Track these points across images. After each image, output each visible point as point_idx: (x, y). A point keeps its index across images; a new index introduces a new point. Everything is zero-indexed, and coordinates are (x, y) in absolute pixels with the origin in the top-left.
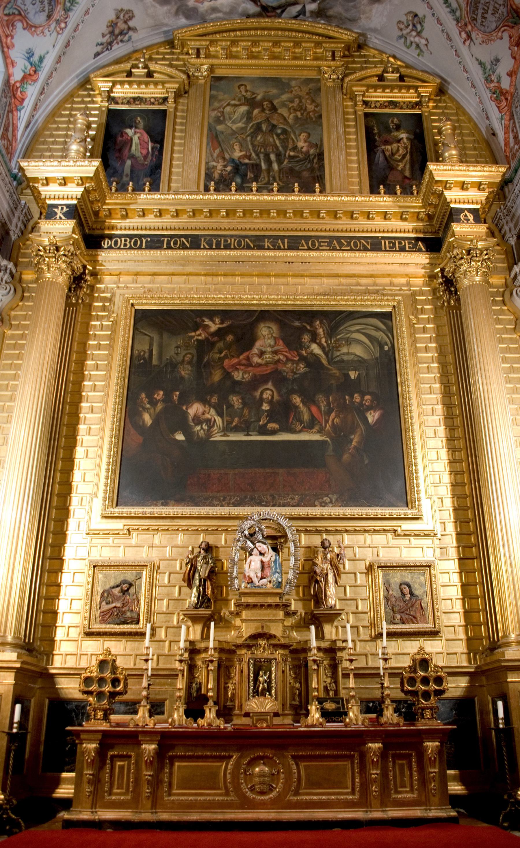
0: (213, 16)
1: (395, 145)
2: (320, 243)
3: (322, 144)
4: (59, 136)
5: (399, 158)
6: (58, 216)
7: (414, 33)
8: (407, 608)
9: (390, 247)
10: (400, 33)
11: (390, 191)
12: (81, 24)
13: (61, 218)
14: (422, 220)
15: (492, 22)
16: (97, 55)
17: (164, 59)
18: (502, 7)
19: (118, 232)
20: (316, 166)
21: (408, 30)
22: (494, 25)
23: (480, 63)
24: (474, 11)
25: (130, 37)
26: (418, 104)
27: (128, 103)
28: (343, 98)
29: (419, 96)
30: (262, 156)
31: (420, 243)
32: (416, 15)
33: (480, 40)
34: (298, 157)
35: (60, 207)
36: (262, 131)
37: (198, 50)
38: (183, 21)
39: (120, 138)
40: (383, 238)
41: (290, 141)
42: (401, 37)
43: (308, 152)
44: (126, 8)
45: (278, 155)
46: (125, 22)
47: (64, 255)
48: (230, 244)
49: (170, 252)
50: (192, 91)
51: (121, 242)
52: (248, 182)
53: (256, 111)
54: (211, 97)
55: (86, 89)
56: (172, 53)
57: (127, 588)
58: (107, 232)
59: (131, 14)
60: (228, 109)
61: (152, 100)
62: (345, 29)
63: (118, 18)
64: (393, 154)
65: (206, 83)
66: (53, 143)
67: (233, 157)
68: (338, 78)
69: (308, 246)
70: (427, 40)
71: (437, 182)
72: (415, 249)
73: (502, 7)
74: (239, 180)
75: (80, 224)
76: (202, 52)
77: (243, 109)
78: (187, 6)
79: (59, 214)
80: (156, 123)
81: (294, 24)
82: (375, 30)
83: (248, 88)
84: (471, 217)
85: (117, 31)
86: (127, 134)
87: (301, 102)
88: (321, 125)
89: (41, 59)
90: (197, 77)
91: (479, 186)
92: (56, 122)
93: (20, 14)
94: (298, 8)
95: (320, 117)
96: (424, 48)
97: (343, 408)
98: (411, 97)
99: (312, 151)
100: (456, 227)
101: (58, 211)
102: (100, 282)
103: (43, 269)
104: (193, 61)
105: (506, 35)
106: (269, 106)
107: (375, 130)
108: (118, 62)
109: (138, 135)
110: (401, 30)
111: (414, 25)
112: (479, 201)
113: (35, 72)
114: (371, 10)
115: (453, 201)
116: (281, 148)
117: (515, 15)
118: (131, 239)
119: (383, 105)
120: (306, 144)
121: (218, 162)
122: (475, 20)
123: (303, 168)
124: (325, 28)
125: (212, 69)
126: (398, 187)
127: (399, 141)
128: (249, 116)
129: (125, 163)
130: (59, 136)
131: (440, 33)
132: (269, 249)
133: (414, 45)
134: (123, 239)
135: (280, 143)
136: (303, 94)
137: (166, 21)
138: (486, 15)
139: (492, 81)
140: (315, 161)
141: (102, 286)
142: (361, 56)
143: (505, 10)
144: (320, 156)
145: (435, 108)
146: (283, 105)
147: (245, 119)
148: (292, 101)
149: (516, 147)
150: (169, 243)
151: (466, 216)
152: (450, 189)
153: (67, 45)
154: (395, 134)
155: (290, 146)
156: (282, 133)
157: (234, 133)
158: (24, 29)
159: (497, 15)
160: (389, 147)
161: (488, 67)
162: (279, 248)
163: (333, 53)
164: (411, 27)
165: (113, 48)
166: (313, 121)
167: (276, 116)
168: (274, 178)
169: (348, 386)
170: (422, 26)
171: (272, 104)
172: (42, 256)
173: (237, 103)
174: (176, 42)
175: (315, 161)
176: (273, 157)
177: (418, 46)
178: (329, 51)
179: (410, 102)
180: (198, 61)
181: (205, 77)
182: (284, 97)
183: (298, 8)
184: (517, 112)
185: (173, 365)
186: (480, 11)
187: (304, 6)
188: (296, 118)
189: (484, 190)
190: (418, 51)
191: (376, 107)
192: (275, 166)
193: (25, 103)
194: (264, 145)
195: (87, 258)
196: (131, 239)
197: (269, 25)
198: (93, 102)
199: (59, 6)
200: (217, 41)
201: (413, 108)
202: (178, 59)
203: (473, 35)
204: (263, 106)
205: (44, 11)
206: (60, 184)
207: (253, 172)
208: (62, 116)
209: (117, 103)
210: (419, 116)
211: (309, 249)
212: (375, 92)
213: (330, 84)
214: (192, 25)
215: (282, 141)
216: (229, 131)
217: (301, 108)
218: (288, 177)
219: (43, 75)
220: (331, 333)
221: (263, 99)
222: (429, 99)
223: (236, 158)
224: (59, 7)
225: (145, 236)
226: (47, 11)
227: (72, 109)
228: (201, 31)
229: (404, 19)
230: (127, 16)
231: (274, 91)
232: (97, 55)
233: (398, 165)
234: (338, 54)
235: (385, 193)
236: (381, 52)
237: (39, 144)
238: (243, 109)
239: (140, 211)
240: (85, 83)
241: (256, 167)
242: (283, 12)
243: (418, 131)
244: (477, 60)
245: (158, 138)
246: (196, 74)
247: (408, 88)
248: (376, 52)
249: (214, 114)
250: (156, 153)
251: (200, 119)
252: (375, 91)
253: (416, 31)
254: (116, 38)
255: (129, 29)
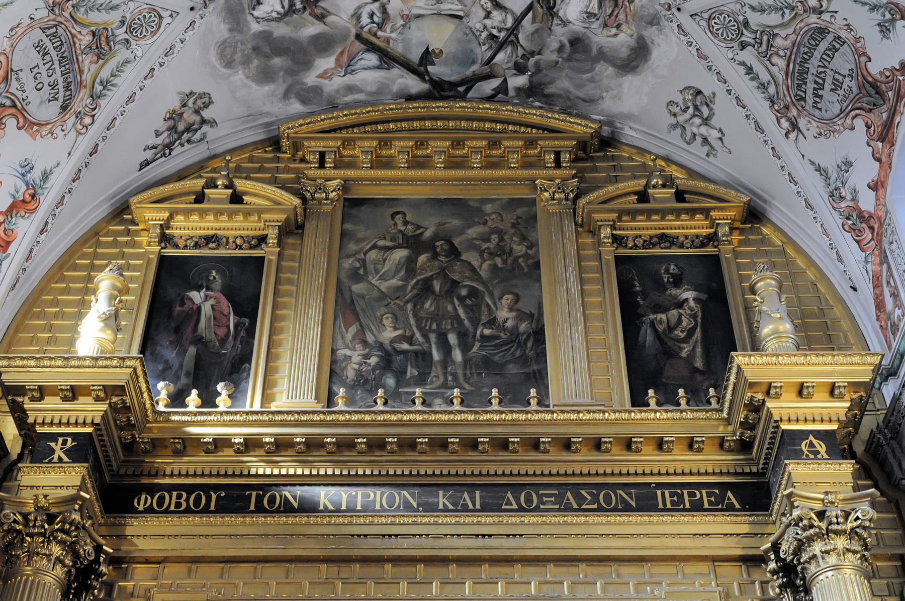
0: (349, 98)
1: (674, 313)
2: (540, 497)
3: (541, 314)
4: (69, 304)
5: (683, 335)
6: (56, 457)
7: (697, 121)
9: (672, 502)
10: (673, 121)
11: (668, 399)
12: (119, 118)
13: (60, 460)
14: (730, 451)
15: (832, 103)
16: (147, 163)
17: (260, 170)
18: (847, 79)
19: (167, 481)
20: (531, 353)
21: (687, 116)
22: (836, 109)
23: (819, 169)
24: (799, 86)
25: (204, 136)
26: (712, 239)
27: (197, 245)
28: (577, 233)
29: (713, 224)
30: (433, 337)
31: (729, 494)
32: (699, 92)
33: (814, 131)
34: (498, 337)
35: (61, 440)
36: (433, 292)
37: (322, 155)
38: (296, 107)
39: (178, 308)
40: (659, 485)
41: (484, 308)
42: (675, 126)
43: (516, 327)
44: (198, 90)
45: (463, 336)
46: (197, 112)
47: (62, 530)
48: (374, 501)
49: (261, 519)
50: (310, 227)
51: (170, 500)
52: (408, 385)
53: (422, 258)
54: (344, 234)
55: (123, 222)
56: (278, 160)
58: (145, 481)
59: (207, 100)
60: (373, 255)
61: (239, 241)
62: (578, 116)
63: (184, 106)
64: (671, 329)
65: (334, 210)
66: (56, 316)
67: (381, 339)
68: (567, 199)
69: (519, 504)
70: (720, 130)
71: (752, 385)
72: (720, 506)
73: (847, 79)
74: (390, 381)
75: (96, 471)
76: (329, 159)
77: (400, 254)
78: (303, 83)
79: (59, 453)
80: (243, 282)
81: (489, 109)
82: (629, 116)
83: (408, 218)
84: (822, 448)
85: (181, 127)
86: (191, 300)
87: (501, 239)
88: (539, 280)
89: (46, 176)
90: (319, 200)
91: (832, 390)
92: (63, 279)
93: (14, 106)
94: (495, 83)
95: (537, 265)
96: (716, 144)
98: (699, 227)
99: (523, 327)
100: (793, 467)
101: (57, 447)
102: (125, 576)
103: (18, 557)
104: (310, 173)
105: (859, 123)
106: (446, 247)
107: (638, 285)
108: (181, 176)
109: (212, 302)
110: (675, 115)
111: (696, 108)
112: (834, 418)
113: (33, 196)
114: (620, 86)
115: (785, 418)
116: (466, 322)
117: (873, 92)
118: (189, 495)
119: (650, 243)
120: (513, 314)
121: (354, 349)
122: (804, 99)
123: (508, 357)
124: (541, 116)
125: (346, 186)
126: (681, 392)
127: (680, 304)
128: (410, 265)
129: (185, 351)
130: (69, 304)
131: (744, 120)
132: (446, 510)
133: (699, 140)
134: (175, 494)
135: (466, 313)
136: (506, 225)
137: (267, 108)
138: (820, 92)
139: (842, 198)
140: (529, 345)
141: (129, 584)
142: (605, 158)
143: (853, 84)
144: (539, 335)
145: (741, 243)
146: (471, 245)
147: (403, 273)
148: (488, 240)
149: (898, 312)
150: (259, 499)
151: (811, 445)
152: (778, 396)
153: (94, 151)
154: (674, 292)
155: (484, 319)
156: (469, 296)
157: (383, 296)
158: (19, 128)
159: (841, 92)
160: (663, 316)
161: (834, 176)
162: (465, 509)
163: (557, 155)
164: (691, 110)
165: (173, 153)
166: (524, 272)
167: (458, 266)
168: (455, 376)
170: (711, 109)
171: (452, 245)
172: (19, 532)
173: (389, 244)
174: (285, 142)
175: (529, 345)
176: (452, 338)
177: (705, 140)
178: (550, 152)
179: (697, 237)
180: (322, 172)
181: (332, 200)
182: (473, 232)
183: (495, 83)
184: (892, 251)
186: (810, 86)
187: (505, 81)
188: (494, 267)
189: (841, 397)
190: (706, 149)
191: (635, 246)
192: (457, 355)
193: (12, 249)
194: (435, 317)
195: (104, 530)
196: (189, 495)
197: (445, 111)
198: (134, 245)
199: (83, 91)
200: (354, 140)
201: (703, 245)
202: (287, 170)
203: (802, 123)
204: (435, 248)
205: (57, 99)
206: (65, 399)
207: (417, 366)
208: (76, 268)
209: (176, 246)
210: (717, 257)
211: (521, 509)
212: (634, 220)
213: (553, 208)
214: (312, 114)
215: (469, 309)
216: (375, 294)
217: (502, 251)
218: (480, 374)
219: (47, 201)
221: (436, 237)
222: (732, 229)
223: (387, 342)
224: (84, 93)
225: (216, 488)
226: (61, 99)
227: (96, 256)
228: (326, 124)
229: (679, 99)
230: (199, 103)
231: (455, 222)
232: (145, 164)
233: (682, 349)
234: (565, 157)
235: (659, 404)
236: (642, 151)
237: (31, 319)
238: (400, 254)
240: (121, 212)
241: (422, 358)
242: (468, 90)
243: (714, 285)
244: (813, 163)
245: (246, 307)
246: (317, 195)
247: (692, 212)
248: (634, 151)
249: (348, 264)
250: (243, 334)
251: (322, 272)
252: (634, 219)
253: (701, 117)
254: (179, 138)
255: (203, 121)
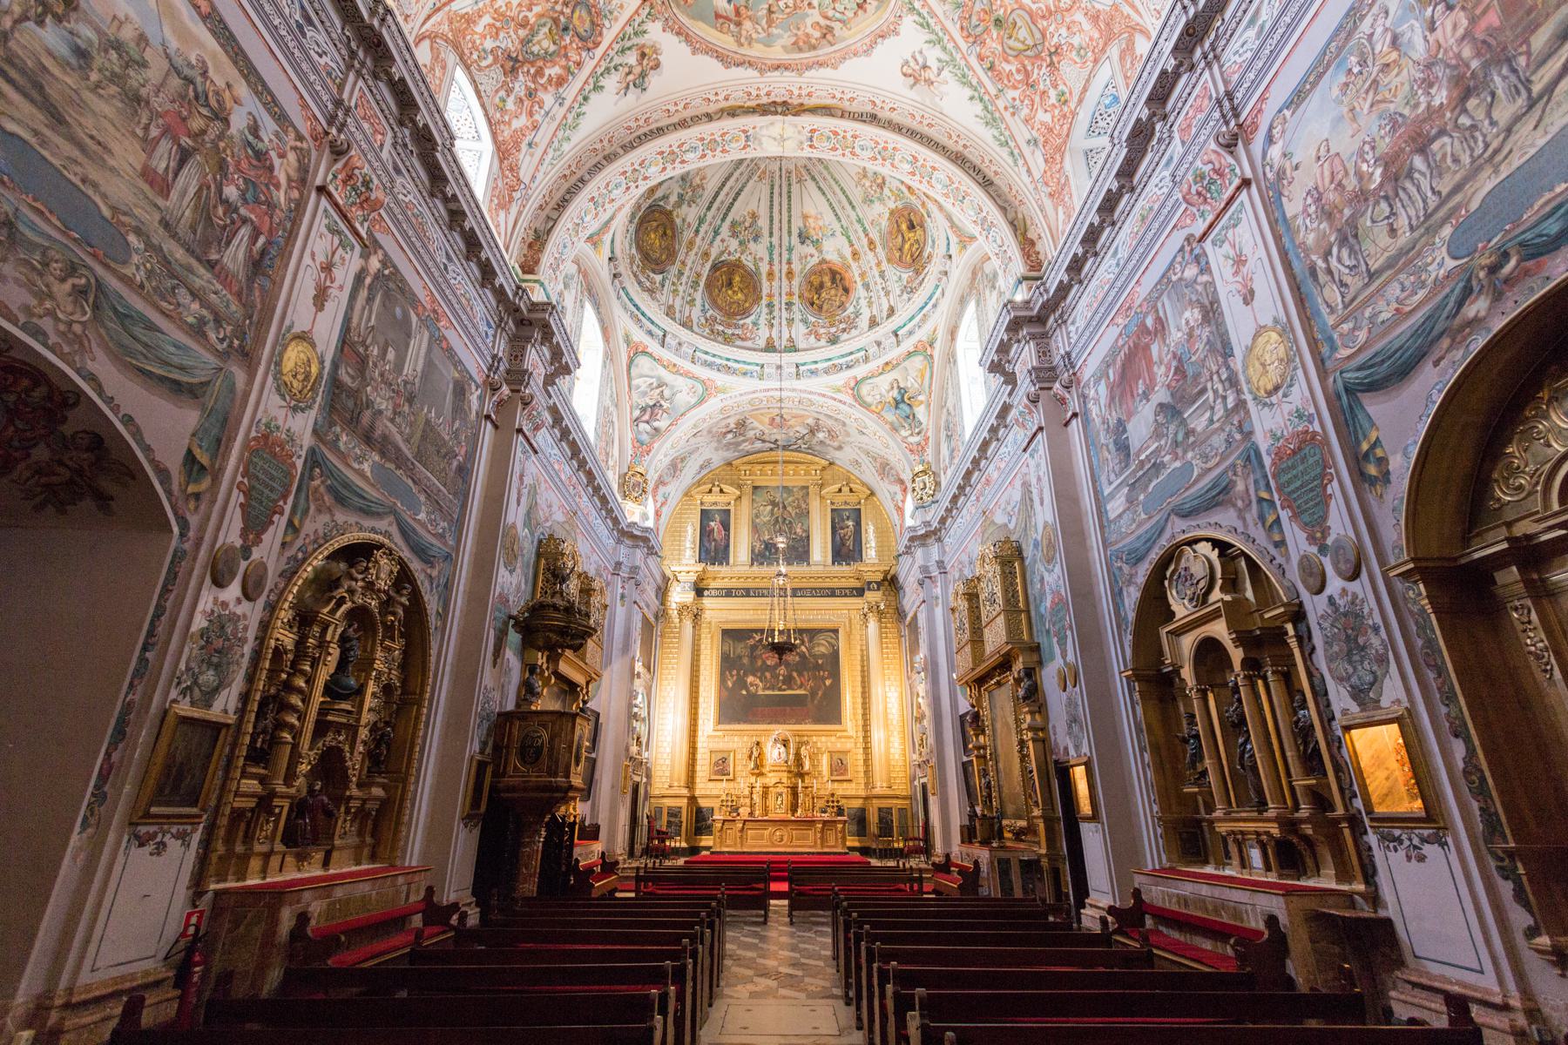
8: (839, 767)
44: (654, 80)
57: (724, 760)
97: (815, 678)
169: (818, 667)
185: (740, 657)
217: (799, 507)
220: (811, 641)
239: (722, 575)
